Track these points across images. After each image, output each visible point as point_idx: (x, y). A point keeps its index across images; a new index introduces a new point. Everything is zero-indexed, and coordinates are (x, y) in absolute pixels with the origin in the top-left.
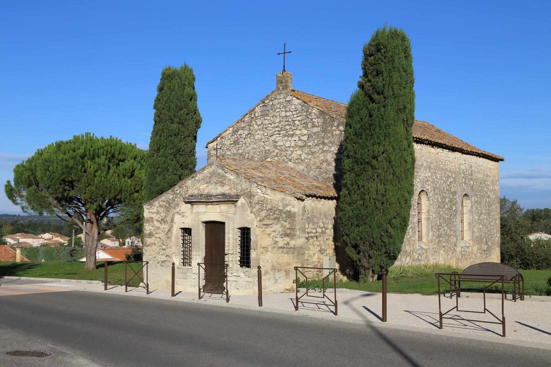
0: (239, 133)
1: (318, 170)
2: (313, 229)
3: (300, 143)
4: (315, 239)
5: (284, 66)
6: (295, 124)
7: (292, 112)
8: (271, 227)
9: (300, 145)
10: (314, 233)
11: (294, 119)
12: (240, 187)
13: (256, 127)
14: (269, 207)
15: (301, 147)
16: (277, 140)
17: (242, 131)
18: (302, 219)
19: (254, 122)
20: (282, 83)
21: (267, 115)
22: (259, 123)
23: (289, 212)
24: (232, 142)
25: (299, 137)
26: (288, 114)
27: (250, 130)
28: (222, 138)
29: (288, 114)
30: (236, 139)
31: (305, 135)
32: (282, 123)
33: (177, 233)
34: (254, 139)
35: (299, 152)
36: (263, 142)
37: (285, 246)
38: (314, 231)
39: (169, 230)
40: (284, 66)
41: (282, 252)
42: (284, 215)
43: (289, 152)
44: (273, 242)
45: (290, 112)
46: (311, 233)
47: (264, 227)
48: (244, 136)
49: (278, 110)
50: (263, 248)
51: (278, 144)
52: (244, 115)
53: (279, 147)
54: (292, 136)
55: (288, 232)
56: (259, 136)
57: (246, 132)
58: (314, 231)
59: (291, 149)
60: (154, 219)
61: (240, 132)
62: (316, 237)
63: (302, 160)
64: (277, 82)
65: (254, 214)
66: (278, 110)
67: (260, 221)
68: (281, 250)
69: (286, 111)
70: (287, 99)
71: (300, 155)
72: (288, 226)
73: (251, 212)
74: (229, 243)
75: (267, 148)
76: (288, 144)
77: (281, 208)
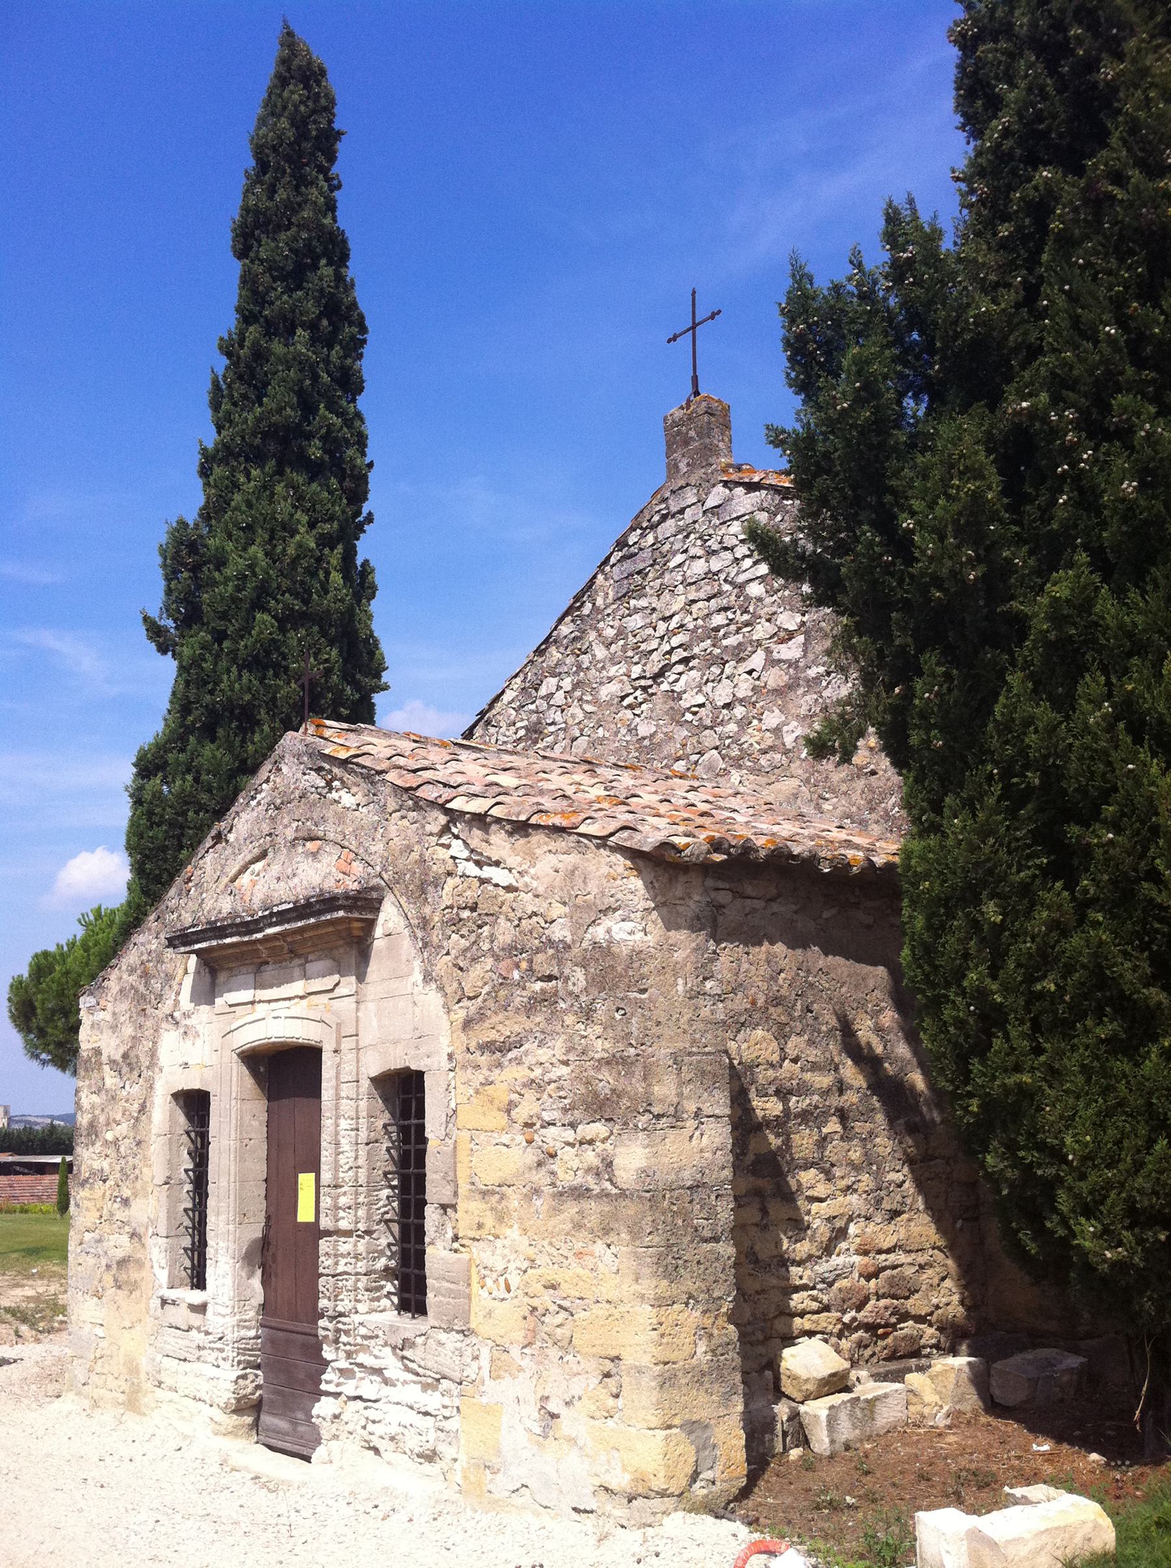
0: (543, 691)
1: (860, 784)
2: (814, 1067)
3: (775, 678)
4: (833, 1126)
5: (695, 380)
6: (748, 598)
7: (732, 549)
8: (519, 1061)
9: (771, 684)
10: (826, 1093)
11: (741, 578)
12: (378, 847)
13: (600, 652)
14: (505, 933)
15: (778, 692)
16: (678, 688)
17: (553, 681)
18: (695, 995)
19: (592, 635)
20: (687, 442)
21: (639, 592)
22: (610, 633)
23: (603, 951)
24: (522, 733)
25: (768, 651)
26: (715, 564)
27: (579, 667)
28: (488, 723)
29: (715, 564)
30: (534, 717)
31: (791, 635)
32: (695, 608)
33: (163, 1115)
34: (595, 702)
35: (772, 719)
36: (630, 707)
37: (591, 1181)
38: (823, 1080)
39: (143, 1109)
40: (695, 380)
41: (578, 1226)
42: (579, 976)
43: (732, 727)
44: (531, 1157)
45: (727, 555)
46: (803, 1090)
47: (484, 1059)
48: (559, 698)
49: (679, 558)
50: (484, 1194)
51: (684, 704)
52: (559, 615)
53: (688, 717)
54: (739, 654)
55: (606, 1081)
56: (613, 688)
57: (567, 683)
58: (823, 1080)
59: (739, 711)
60: (104, 1059)
61: (549, 684)
62: (843, 1115)
63: (786, 752)
64: (669, 445)
65: (441, 988)
66: (679, 558)
67: (467, 1024)
68: (571, 1209)
69: (711, 553)
70: (711, 502)
71: (777, 731)
72: (601, 1048)
73: (428, 977)
74: (336, 1167)
75: (644, 729)
76: (722, 694)
77: (559, 932)
